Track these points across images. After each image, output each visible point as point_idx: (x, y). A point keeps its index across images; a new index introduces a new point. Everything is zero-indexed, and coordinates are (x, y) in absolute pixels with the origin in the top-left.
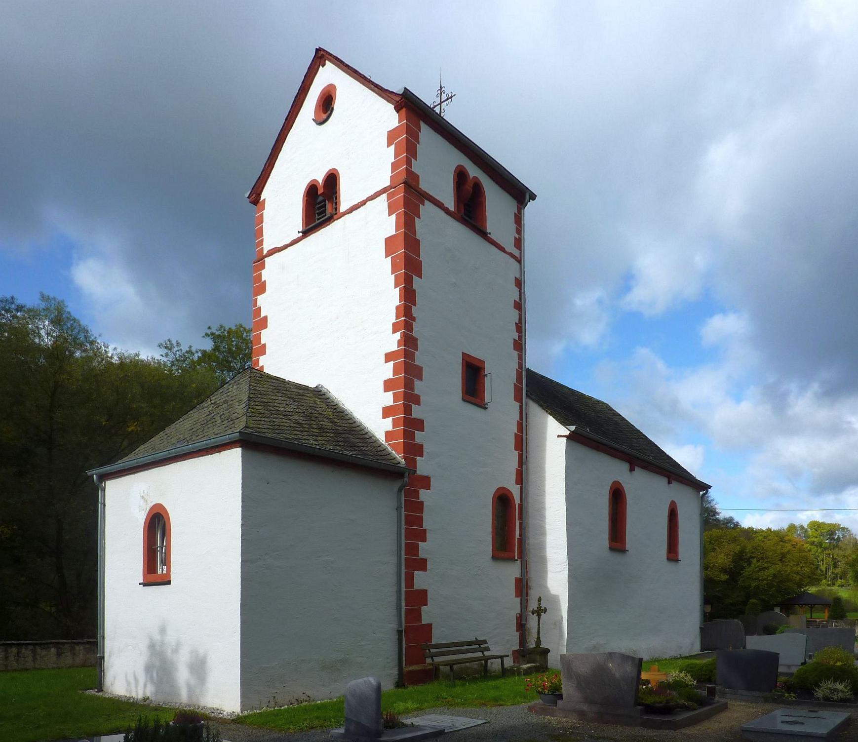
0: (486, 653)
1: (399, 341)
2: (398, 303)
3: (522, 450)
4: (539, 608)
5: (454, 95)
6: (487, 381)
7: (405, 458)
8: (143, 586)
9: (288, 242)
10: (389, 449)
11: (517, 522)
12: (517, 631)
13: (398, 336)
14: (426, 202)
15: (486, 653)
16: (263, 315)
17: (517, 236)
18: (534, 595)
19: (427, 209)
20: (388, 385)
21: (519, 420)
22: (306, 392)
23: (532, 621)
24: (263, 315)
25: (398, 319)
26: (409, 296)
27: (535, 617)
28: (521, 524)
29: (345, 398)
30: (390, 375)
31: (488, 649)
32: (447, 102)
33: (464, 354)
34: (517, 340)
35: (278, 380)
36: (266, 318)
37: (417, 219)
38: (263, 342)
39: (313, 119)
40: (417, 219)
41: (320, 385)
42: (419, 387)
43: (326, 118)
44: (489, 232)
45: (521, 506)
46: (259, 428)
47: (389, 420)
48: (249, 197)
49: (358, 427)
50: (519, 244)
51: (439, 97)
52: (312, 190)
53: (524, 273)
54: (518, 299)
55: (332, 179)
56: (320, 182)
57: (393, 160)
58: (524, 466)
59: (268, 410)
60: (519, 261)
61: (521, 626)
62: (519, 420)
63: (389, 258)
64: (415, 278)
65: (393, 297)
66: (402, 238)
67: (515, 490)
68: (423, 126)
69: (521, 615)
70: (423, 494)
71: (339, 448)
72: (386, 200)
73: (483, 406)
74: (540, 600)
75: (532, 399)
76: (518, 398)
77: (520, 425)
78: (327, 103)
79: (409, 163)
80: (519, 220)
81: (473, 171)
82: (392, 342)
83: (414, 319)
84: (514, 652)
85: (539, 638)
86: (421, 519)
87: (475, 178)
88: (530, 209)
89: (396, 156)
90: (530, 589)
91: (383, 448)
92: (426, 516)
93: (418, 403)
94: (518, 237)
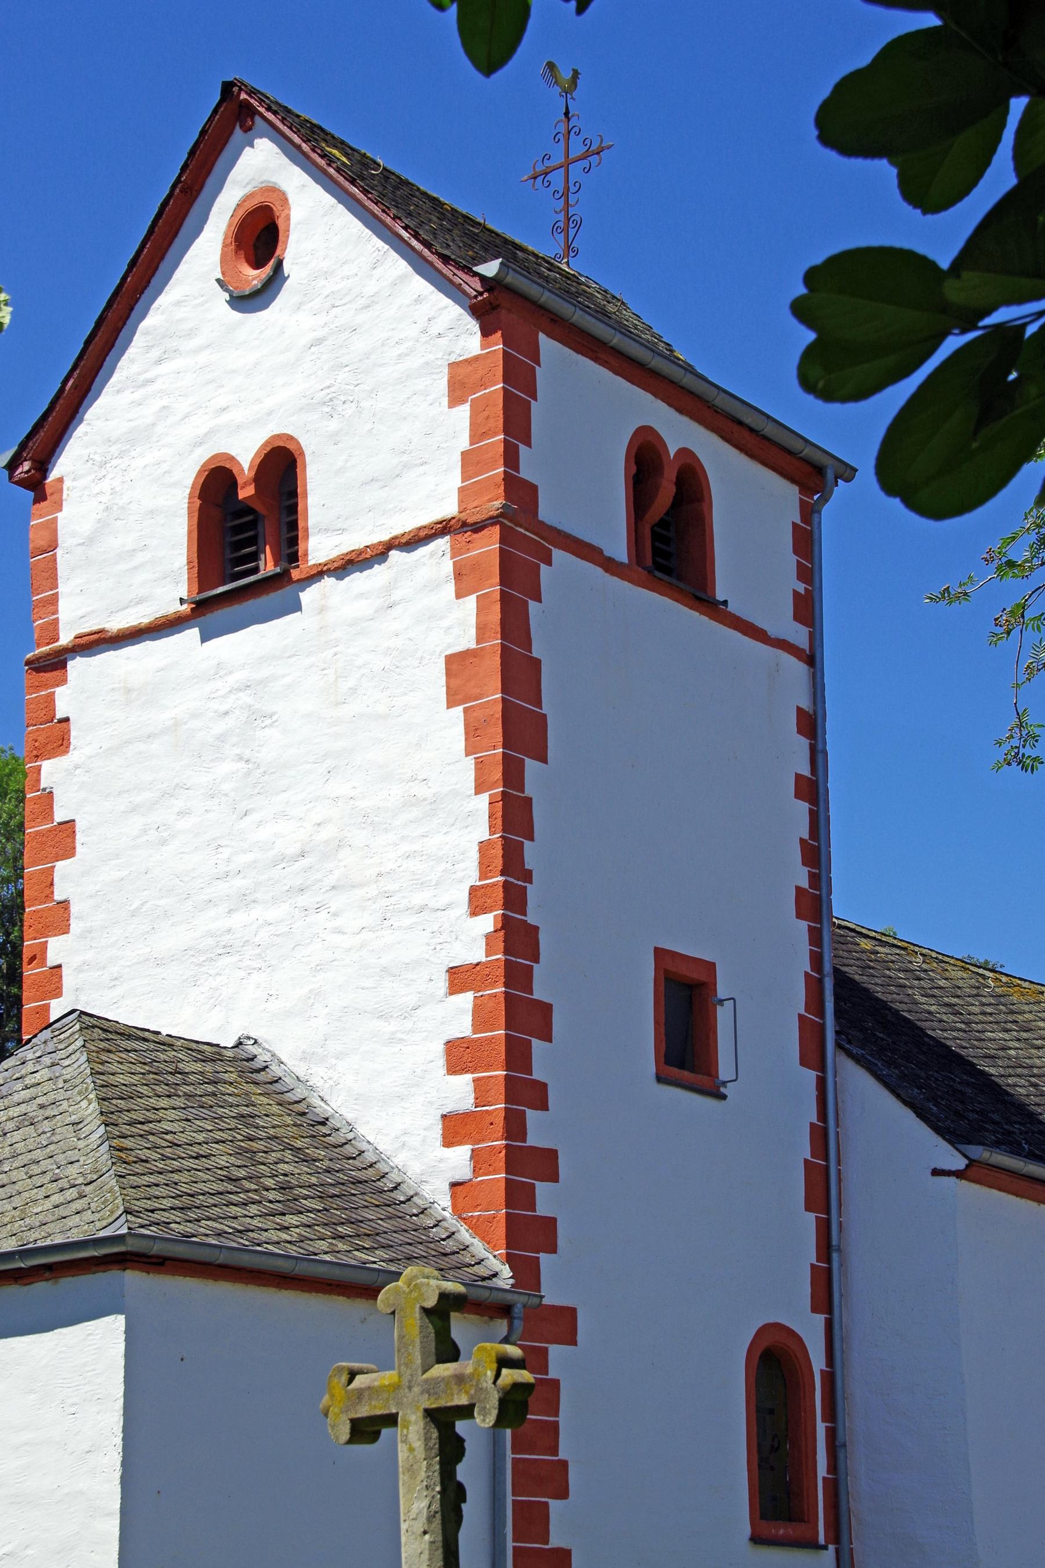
1: (488, 937)
2: (485, 835)
3: (828, 1212)
5: (609, 147)
6: (723, 1016)
7: (510, 1259)
10: (465, 1235)
11: (821, 1428)
13: (487, 922)
14: (558, 555)
16: (60, 815)
17: (801, 588)
21: (815, 1121)
24: (59, 816)
25: (487, 878)
28: (832, 1434)
29: (331, 1082)
30: (463, 1027)
32: (585, 163)
33: (660, 953)
34: (806, 840)
35: (145, 1040)
36: (69, 825)
37: (532, 605)
39: (218, 281)
40: (532, 605)
41: (249, 1038)
43: (256, 284)
44: (721, 600)
45: (830, 1379)
46: (152, 1211)
47: (462, 1153)
49: (371, 1166)
51: (571, 184)
53: (840, 1180)
54: (806, 704)
56: (246, 466)
58: (835, 1256)
59: (155, 1147)
60: (811, 659)
62: (815, 1121)
63: (458, 710)
64: (531, 765)
66: (495, 662)
68: (546, 344)
71: (341, 1246)
72: (448, 555)
75: (849, 1054)
77: (820, 1137)
79: (511, 458)
83: (528, 876)
87: (684, 452)
89: (477, 433)
91: (446, 1229)
94: (803, 592)
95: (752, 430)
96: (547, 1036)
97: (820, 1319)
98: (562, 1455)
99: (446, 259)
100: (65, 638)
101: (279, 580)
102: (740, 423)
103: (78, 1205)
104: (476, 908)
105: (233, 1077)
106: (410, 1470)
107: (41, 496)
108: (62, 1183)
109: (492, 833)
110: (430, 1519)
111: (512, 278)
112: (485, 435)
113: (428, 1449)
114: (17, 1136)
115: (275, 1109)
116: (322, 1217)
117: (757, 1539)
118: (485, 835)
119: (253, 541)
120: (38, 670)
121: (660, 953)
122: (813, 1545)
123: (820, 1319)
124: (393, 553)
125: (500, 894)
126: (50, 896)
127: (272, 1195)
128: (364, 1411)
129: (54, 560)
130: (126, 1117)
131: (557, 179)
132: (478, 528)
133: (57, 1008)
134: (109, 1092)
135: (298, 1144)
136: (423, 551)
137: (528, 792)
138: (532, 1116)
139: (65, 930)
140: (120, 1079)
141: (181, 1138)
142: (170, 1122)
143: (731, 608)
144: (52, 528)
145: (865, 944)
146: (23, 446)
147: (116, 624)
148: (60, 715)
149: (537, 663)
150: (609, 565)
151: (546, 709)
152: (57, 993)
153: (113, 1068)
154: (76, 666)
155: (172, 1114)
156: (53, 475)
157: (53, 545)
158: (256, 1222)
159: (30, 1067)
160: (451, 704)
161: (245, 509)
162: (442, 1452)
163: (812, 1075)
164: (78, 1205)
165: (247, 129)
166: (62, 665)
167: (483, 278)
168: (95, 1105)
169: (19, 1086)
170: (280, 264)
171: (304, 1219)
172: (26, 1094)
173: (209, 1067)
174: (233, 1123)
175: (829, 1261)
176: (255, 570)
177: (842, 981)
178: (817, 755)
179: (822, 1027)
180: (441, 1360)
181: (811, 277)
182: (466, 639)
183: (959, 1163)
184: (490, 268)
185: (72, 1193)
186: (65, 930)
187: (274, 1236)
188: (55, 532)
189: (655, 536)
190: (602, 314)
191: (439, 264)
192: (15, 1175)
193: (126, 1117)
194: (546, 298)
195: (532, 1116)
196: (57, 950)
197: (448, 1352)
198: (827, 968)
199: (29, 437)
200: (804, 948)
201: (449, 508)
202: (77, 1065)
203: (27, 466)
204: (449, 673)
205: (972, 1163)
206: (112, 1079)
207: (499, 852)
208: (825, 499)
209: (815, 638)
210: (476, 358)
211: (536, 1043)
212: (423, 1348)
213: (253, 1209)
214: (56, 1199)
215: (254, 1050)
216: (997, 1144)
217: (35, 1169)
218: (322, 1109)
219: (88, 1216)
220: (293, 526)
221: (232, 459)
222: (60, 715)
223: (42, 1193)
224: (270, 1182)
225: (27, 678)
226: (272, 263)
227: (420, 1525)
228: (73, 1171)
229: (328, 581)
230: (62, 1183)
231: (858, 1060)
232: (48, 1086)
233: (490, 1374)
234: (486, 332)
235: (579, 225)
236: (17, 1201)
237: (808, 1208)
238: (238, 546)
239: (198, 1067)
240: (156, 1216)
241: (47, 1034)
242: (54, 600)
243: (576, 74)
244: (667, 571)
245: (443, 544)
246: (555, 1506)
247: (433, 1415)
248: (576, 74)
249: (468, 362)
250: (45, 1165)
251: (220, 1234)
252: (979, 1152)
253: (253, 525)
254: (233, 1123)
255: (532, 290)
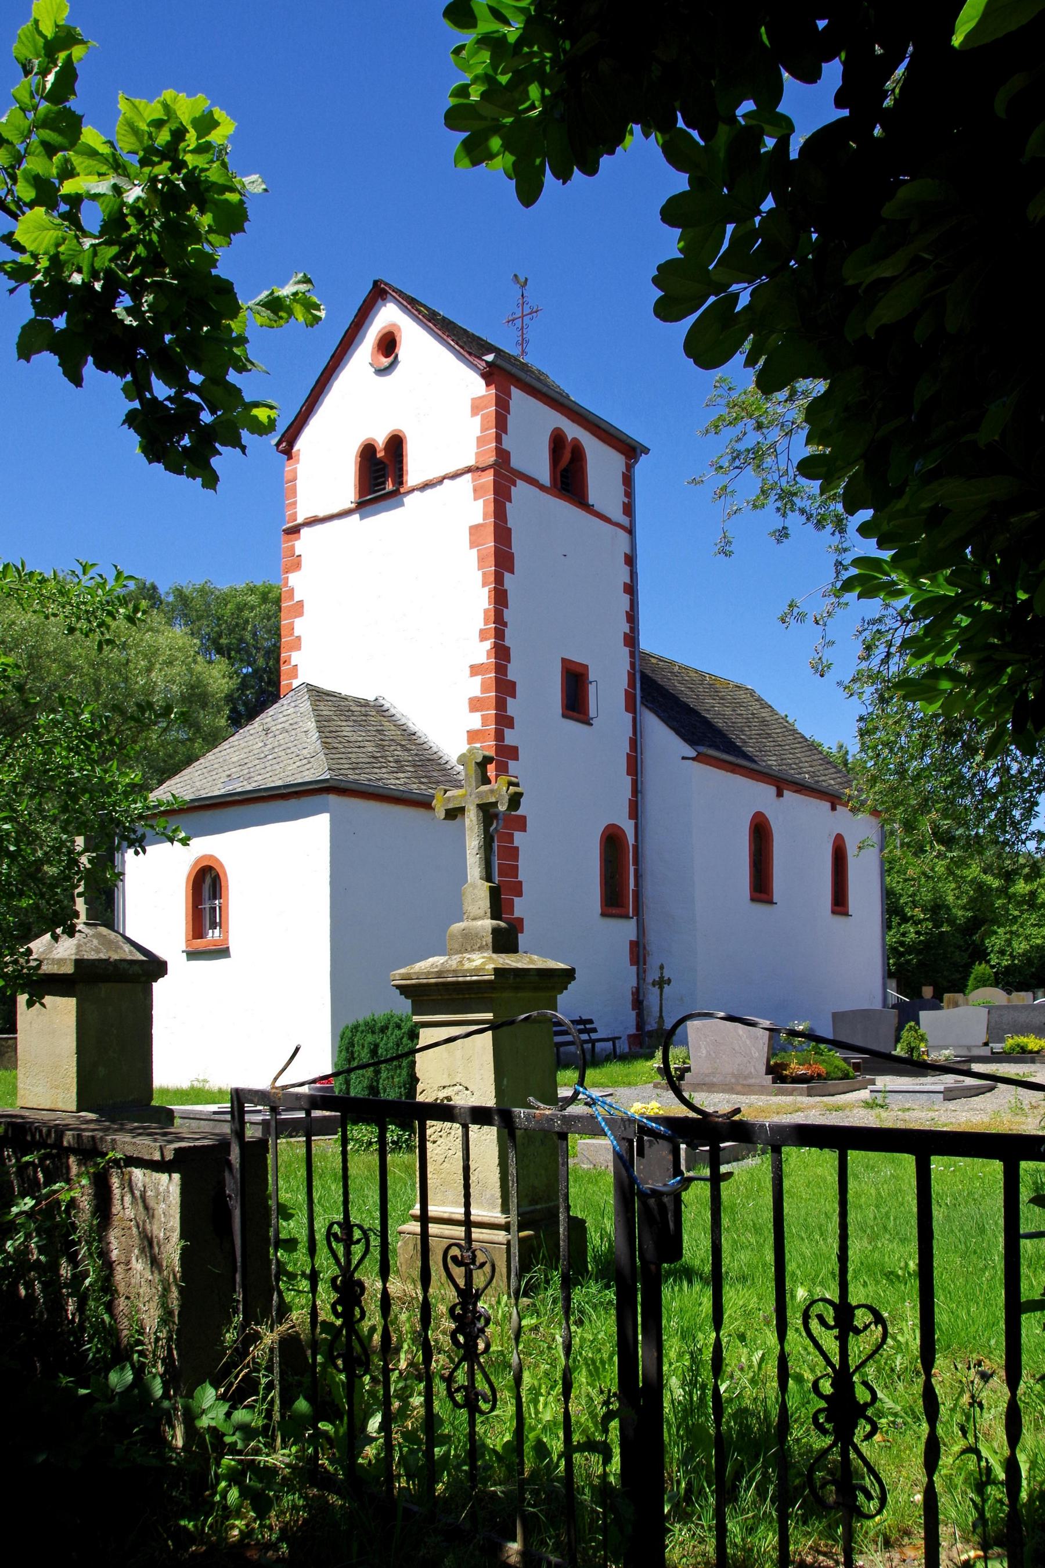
0: (594, 1036)
2: (486, 606)
3: (636, 775)
4: (662, 977)
6: (592, 688)
8: (631, 942)
9: (335, 510)
11: (632, 868)
12: (633, 1009)
13: (488, 644)
14: (519, 482)
15: (594, 1036)
17: (626, 500)
18: (653, 963)
19: (520, 490)
20: (475, 705)
22: (367, 709)
23: (652, 996)
24: (297, 598)
26: (500, 598)
27: (656, 990)
28: (636, 871)
31: (594, 1030)
33: (564, 660)
38: (296, 634)
42: (513, 707)
43: (386, 364)
45: (636, 848)
48: (278, 444)
50: (629, 509)
52: (368, 451)
54: (628, 581)
55: (396, 443)
57: (479, 434)
59: (340, 742)
60: (631, 531)
61: (638, 1003)
63: (475, 551)
64: (507, 575)
65: (481, 599)
67: (628, 827)
68: (515, 392)
69: (638, 988)
70: (519, 838)
71: (423, 787)
73: (587, 721)
74: (662, 967)
75: (647, 707)
76: (631, 706)
77: (634, 743)
78: (388, 344)
79: (498, 439)
80: (628, 480)
81: (573, 431)
82: (482, 652)
83: (505, 625)
84: (629, 1036)
85: (661, 1017)
86: (516, 868)
87: (575, 439)
88: (642, 466)
89: (483, 429)
90: (205, 1081)
92: (522, 863)
93: (511, 726)
95: (604, 430)
96: (514, 696)
97: (632, 822)
98: (519, 879)
99: (470, 354)
100: (300, 520)
101: (395, 493)
102: (599, 427)
103: (308, 766)
104: (483, 639)
105: (374, 713)
106: (471, 829)
107: (290, 458)
108: (301, 757)
109: (486, 624)
110: (480, 848)
111: (499, 362)
112: (487, 429)
113: (478, 820)
114: (281, 737)
115: (393, 728)
116: (414, 775)
117: (604, 914)
118: (486, 606)
119: (383, 476)
120: (288, 534)
121: (564, 660)
122: (626, 916)
123: (632, 822)
124: (446, 481)
125: (493, 632)
126: (292, 634)
127: (392, 764)
128: (451, 806)
129: (295, 485)
130: (328, 729)
131: (518, 322)
132: (483, 470)
133: (295, 683)
134: (320, 718)
135: (403, 743)
136: (459, 480)
137: (506, 587)
138: (507, 731)
139: (299, 649)
140: (325, 713)
141: (352, 739)
142: (347, 731)
143: (595, 508)
144: (295, 471)
145: (654, 661)
146: (283, 436)
147: (321, 514)
148: (297, 554)
149: (510, 530)
150: (542, 488)
151: (515, 549)
152: (296, 677)
153: (322, 708)
154: (304, 531)
155: (348, 729)
156: (295, 449)
157: (295, 479)
158: (385, 776)
159: (285, 707)
160: (471, 547)
161: (380, 462)
162: (484, 822)
163: (631, 715)
164: (308, 766)
165: (384, 299)
166: (298, 531)
167: (486, 362)
168: (314, 724)
169: (281, 715)
170: (397, 356)
171: (405, 775)
172: (284, 719)
173: (363, 709)
174: (374, 733)
175: (636, 797)
176: (384, 489)
177: (644, 676)
178: (633, 575)
179: (635, 694)
180: (483, 784)
181: (660, 268)
182: (478, 519)
183: (694, 754)
184: (490, 358)
185: (305, 761)
186: (299, 649)
187: (393, 781)
188: (296, 473)
189: (562, 476)
190: (539, 380)
191: (467, 356)
192: (280, 754)
193: (328, 729)
194: (514, 371)
195: (507, 731)
196: (296, 658)
197: (486, 781)
198: (637, 668)
199: (286, 432)
200: (627, 660)
201: (471, 461)
202: (306, 706)
203: (284, 444)
204: (471, 534)
205: (699, 754)
206: (321, 713)
207: (493, 613)
208: (636, 462)
209: (632, 523)
210: (484, 396)
211: (508, 698)
212: (476, 778)
213: (384, 770)
214: (298, 764)
215: (383, 702)
216: (710, 746)
217: (289, 751)
218: (413, 728)
219: (312, 771)
220: (401, 469)
221: (374, 440)
222: (297, 554)
223: (292, 761)
224: (391, 759)
225: (283, 537)
226: (393, 355)
227: (475, 851)
228: (305, 752)
229: (416, 493)
230: (301, 757)
231: (651, 709)
232: (293, 716)
233: (505, 789)
234: (488, 385)
235: (528, 342)
236: (281, 765)
237: (628, 774)
238: (377, 478)
239: (359, 709)
240: (342, 772)
241: (292, 693)
242: (295, 503)
243: (526, 279)
244: (568, 491)
245: (468, 477)
246: (516, 900)
247: (480, 807)
248: (526, 279)
249: (480, 398)
250: (293, 749)
251: (370, 780)
252: (703, 749)
253: (383, 469)
254: (374, 733)
255: (508, 367)
